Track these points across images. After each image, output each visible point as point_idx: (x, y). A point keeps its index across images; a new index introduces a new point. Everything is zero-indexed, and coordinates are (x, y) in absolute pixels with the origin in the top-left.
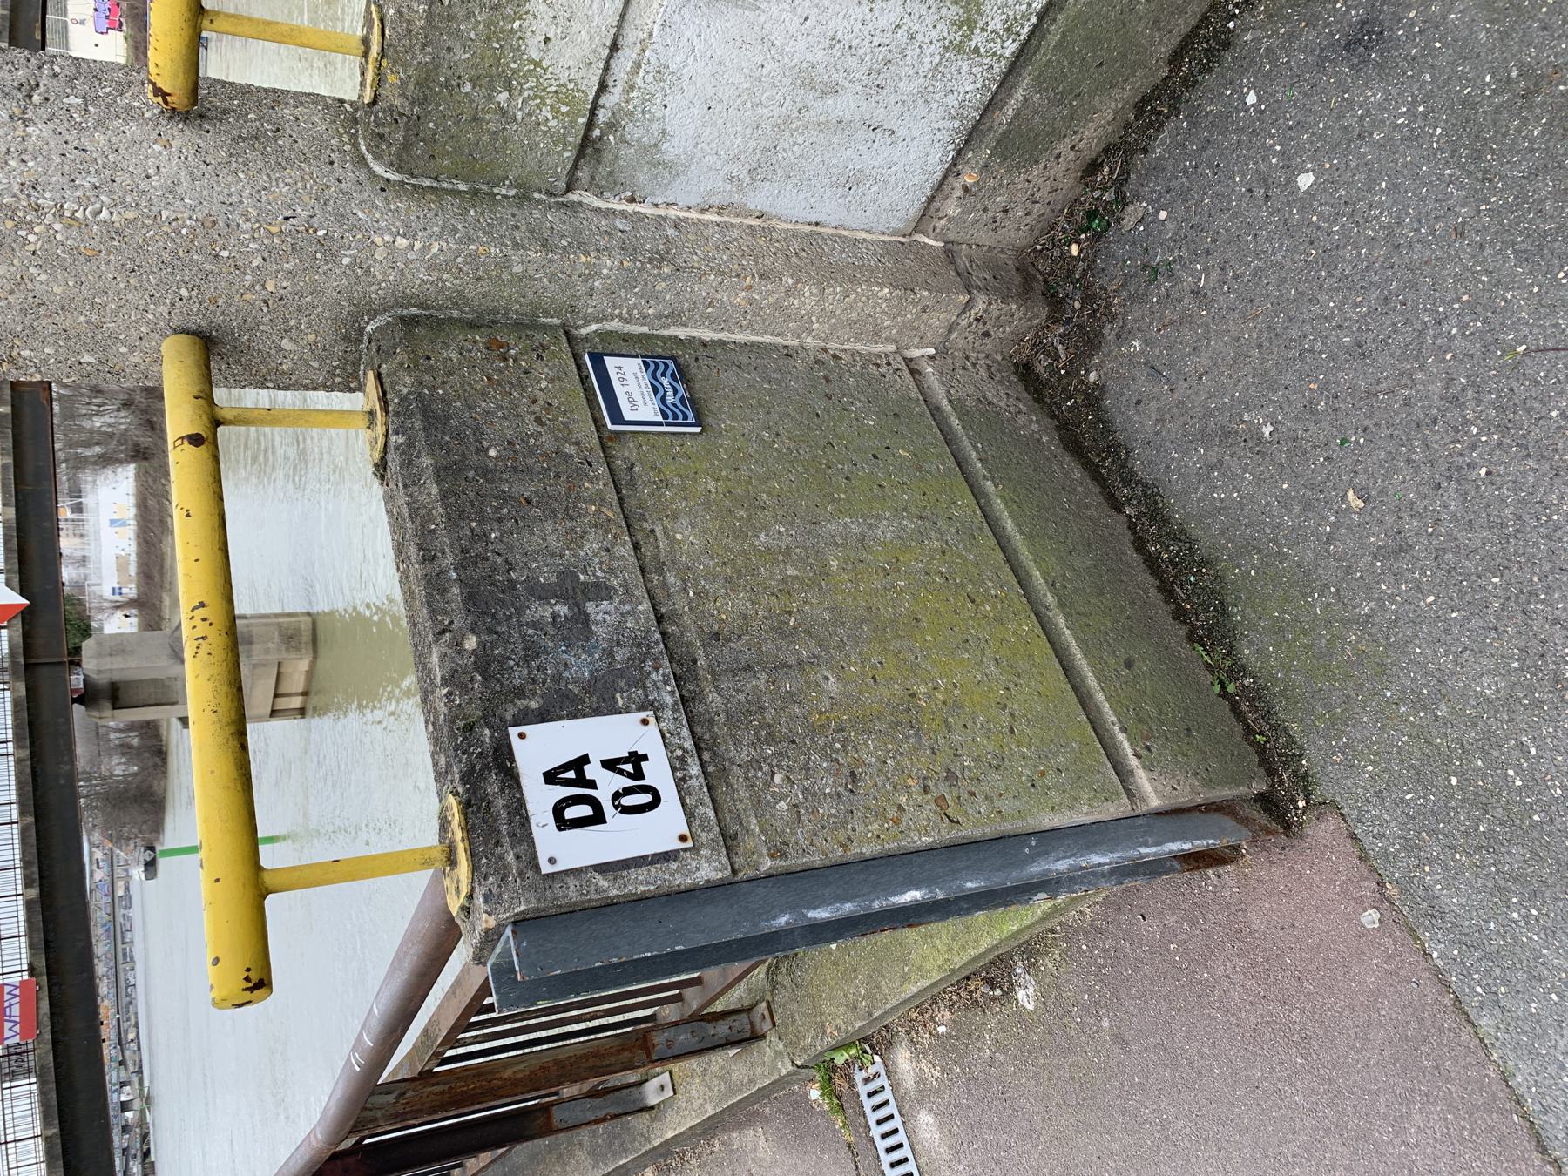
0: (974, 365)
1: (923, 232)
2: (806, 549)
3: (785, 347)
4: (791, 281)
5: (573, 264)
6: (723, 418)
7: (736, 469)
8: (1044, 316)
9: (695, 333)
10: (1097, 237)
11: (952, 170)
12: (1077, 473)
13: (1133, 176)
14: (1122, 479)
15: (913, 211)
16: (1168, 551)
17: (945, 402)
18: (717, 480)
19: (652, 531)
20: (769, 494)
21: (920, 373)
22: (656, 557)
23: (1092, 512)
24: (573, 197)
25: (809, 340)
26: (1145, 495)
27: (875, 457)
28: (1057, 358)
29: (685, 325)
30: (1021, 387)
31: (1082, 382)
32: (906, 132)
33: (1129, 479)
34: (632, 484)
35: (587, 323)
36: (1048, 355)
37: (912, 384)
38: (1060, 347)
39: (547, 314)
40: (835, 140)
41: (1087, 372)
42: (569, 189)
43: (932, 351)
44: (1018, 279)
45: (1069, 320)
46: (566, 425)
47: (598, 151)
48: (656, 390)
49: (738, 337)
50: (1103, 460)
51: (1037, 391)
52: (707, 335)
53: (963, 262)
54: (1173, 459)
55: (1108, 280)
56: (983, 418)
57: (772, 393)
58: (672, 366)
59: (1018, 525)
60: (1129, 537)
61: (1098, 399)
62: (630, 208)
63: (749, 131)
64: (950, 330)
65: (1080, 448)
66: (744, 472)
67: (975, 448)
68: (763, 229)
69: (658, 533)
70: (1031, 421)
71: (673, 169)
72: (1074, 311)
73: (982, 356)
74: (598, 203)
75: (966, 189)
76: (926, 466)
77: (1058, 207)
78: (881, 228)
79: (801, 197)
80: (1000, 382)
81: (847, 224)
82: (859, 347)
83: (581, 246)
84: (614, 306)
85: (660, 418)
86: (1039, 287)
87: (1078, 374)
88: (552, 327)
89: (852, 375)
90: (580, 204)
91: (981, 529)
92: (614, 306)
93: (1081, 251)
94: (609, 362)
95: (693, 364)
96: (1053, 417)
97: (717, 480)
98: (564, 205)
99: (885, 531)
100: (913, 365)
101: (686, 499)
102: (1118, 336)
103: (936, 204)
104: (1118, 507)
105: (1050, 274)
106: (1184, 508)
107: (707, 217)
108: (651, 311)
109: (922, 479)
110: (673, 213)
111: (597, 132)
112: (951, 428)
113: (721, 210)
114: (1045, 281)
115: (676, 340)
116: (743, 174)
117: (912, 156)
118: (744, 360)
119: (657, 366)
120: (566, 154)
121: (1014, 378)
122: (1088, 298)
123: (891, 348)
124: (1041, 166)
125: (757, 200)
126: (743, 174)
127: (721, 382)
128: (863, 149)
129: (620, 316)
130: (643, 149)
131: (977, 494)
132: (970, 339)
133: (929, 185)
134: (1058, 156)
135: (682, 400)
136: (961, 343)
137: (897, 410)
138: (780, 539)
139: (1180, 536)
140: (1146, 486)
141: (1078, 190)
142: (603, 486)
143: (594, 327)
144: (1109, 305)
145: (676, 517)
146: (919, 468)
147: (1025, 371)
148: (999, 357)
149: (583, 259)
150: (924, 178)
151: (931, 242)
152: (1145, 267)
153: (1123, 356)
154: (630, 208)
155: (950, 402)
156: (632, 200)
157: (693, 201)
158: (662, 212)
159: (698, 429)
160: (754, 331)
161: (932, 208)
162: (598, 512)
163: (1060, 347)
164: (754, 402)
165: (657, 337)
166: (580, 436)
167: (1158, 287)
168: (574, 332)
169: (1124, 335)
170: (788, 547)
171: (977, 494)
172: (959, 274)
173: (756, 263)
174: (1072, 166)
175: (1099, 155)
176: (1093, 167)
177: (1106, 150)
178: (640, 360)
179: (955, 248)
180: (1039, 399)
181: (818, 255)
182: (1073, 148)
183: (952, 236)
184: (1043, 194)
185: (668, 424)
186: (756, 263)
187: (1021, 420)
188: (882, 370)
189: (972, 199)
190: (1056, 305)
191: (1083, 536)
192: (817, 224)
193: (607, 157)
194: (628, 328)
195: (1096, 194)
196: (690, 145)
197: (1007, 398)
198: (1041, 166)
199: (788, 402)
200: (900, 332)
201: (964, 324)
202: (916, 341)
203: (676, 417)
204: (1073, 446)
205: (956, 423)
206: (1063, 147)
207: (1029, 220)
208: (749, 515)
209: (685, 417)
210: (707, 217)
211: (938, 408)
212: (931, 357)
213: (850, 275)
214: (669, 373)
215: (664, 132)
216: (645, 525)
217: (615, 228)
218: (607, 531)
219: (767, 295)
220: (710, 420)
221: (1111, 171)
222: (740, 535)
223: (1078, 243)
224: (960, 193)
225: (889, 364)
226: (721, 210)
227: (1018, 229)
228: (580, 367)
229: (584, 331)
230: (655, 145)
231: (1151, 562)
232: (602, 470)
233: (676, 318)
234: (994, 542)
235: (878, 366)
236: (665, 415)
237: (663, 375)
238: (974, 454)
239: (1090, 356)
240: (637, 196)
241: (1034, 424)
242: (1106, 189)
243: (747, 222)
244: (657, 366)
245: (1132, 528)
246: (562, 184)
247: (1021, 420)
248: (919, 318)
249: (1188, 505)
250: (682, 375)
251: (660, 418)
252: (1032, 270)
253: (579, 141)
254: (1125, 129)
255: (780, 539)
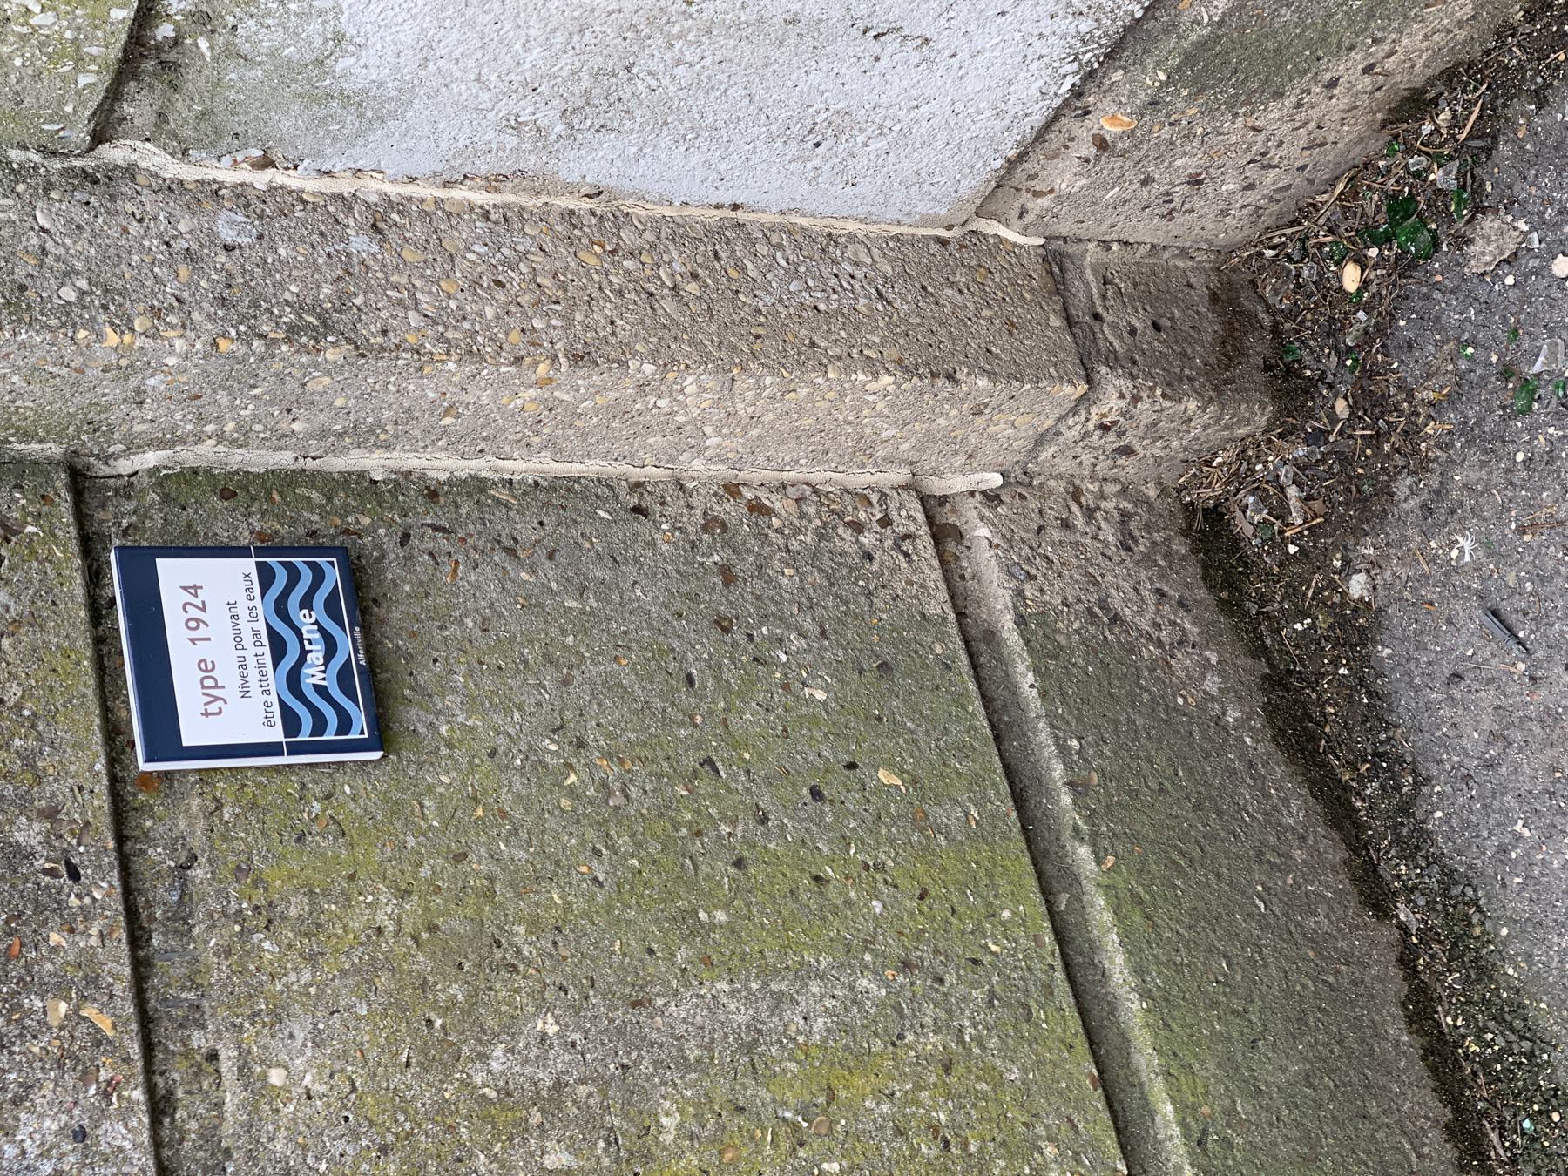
0: (1090, 513)
1: (994, 216)
2: (603, 1083)
3: (637, 486)
4: (649, 368)
5: (85, 351)
6: (446, 710)
7: (460, 857)
8: (1262, 421)
9: (412, 462)
10: (1404, 266)
11: (1075, 103)
12: (1297, 809)
13: (1505, 149)
14: (1398, 840)
15: (974, 183)
16: (1479, 1040)
17: (1007, 623)
18: (404, 894)
19: (213, 1056)
20: (534, 925)
21: (959, 535)
22: (209, 1135)
23: (1320, 922)
24: (114, 153)
25: (697, 464)
26: (1446, 892)
27: (816, 794)
28: (1282, 513)
29: (388, 447)
30: (1193, 570)
31: (1333, 586)
32: (958, 41)
33: (1415, 845)
34: (180, 918)
35: (132, 447)
36: (1264, 498)
37: (934, 576)
38: (1292, 491)
39: (26, 436)
40: (781, 56)
41: (1348, 568)
42: (98, 138)
43: (995, 480)
44: (1212, 327)
45: (1319, 436)
46: (28, 759)
47: (174, 67)
48: (278, 648)
49: (521, 467)
50: (1361, 779)
51: (1231, 584)
52: (441, 464)
53: (1086, 285)
54: (1518, 837)
55: (1424, 369)
56: (1097, 669)
57: (582, 624)
58: (333, 576)
59: (1139, 971)
60: (1398, 986)
61: (1366, 638)
62: (261, 179)
63: (560, 38)
64: (1040, 441)
65: (1314, 738)
66: (479, 864)
67: (1064, 751)
68: (602, 224)
69: (227, 1065)
70: (1206, 666)
71: (369, 109)
72: (1333, 419)
73: (1111, 488)
74: (174, 169)
75: (1102, 144)
76: (939, 814)
77: (1325, 175)
78: (893, 214)
79: (695, 159)
80: (1147, 559)
81: (807, 207)
82: (818, 476)
83: (111, 301)
84: (201, 419)
85: (276, 734)
86: (1258, 347)
87: (1325, 566)
88: (38, 466)
89: (791, 558)
90: (130, 171)
91: (1048, 989)
92: (201, 419)
93: (1365, 285)
94: (171, 573)
95: (394, 552)
96: (1259, 650)
97: (404, 894)
98: (88, 177)
99: (812, 1014)
100: (946, 516)
101: (312, 959)
102: (1427, 509)
103: (1030, 166)
104: (1378, 901)
105: (1289, 315)
106: (1529, 957)
107: (459, 194)
108: (296, 426)
109: (925, 852)
110: (373, 187)
111: (165, 30)
112: (1014, 690)
113: (493, 183)
114: (1276, 330)
115: (361, 486)
116: (548, 116)
117: (972, 86)
118: (526, 531)
119: (294, 575)
120: (83, 80)
121: (1180, 547)
122: (1369, 402)
123: (899, 475)
124: (1290, 101)
125: (590, 163)
126: (548, 116)
127: (454, 604)
128: (848, 71)
129: (220, 437)
130: (286, 70)
131: (1051, 877)
132: (1087, 458)
133: (1014, 136)
134: (1333, 83)
135: (344, 676)
136: (1065, 465)
137: (888, 652)
138: (542, 1061)
139: (1509, 1014)
140: (1449, 873)
141: (1374, 145)
142: (100, 941)
143: (151, 459)
144: (1411, 433)
145: (278, 1016)
146: (920, 822)
147: (1208, 530)
148: (1152, 492)
149: (112, 338)
150: (999, 125)
151: (1012, 236)
152: (1506, 373)
153: (1432, 560)
154: (261, 179)
155: (1021, 621)
156: (266, 163)
157: (423, 166)
158: (345, 186)
159: (377, 755)
160: (559, 453)
161: (1020, 173)
162: (75, 1016)
163: (1292, 491)
164: (532, 654)
165: (312, 478)
166: (62, 789)
167: (1533, 429)
168: (103, 470)
169: (1441, 513)
170: (559, 1085)
171: (1051, 877)
172: (1070, 322)
173: (568, 320)
174: (1365, 101)
175: (1430, 81)
176: (1415, 104)
177: (1449, 76)
178: (249, 565)
179: (1071, 248)
180: (1230, 607)
181: (726, 286)
182: (1368, 70)
183: (1063, 229)
184: (1293, 152)
185: (295, 749)
186: (568, 320)
187: (1184, 662)
188: (867, 540)
189: (1117, 162)
190: (1291, 389)
191: (1288, 993)
192: (735, 207)
193: (194, 82)
194: (238, 458)
195: (1417, 162)
196: (409, 63)
197: (1153, 603)
198: (1290, 101)
199: (620, 645)
200: (919, 447)
201: (1074, 433)
202: (959, 460)
203: (320, 725)
204: (1297, 730)
205: (1026, 679)
206: (1348, 68)
207: (1252, 197)
208: (472, 996)
209: (345, 724)
210: (459, 194)
211: (991, 636)
212: (991, 497)
213: (798, 343)
214: (319, 599)
215: (338, 38)
216: (198, 1040)
217: (212, 235)
218: (86, 1078)
219: (585, 391)
220: (413, 713)
221: (1456, 122)
222: (439, 1057)
223: (1362, 262)
224: (1088, 150)
225: (886, 522)
226: (493, 183)
227: (1225, 213)
228: (95, 576)
229: (125, 466)
230: (319, 63)
231: (1440, 1055)
232: (105, 888)
233: (363, 435)
234: (1075, 1024)
235: (858, 527)
236: (291, 722)
237: (307, 603)
238: (1058, 770)
239: (1359, 533)
240: (276, 155)
241: (1210, 678)
242: (1438, 159)
243: (565, 203)
244: (294, 575)
245: (1406, 962)
246: (79, 134)
247: (1184, 662)
248: (964, 423)
249: (1539, 956)
250: (361, 599)
251: (276, 734)
252: (1247, 301)
253: (115, 52)
254: (1499, 35)
255: (542, 1061)
